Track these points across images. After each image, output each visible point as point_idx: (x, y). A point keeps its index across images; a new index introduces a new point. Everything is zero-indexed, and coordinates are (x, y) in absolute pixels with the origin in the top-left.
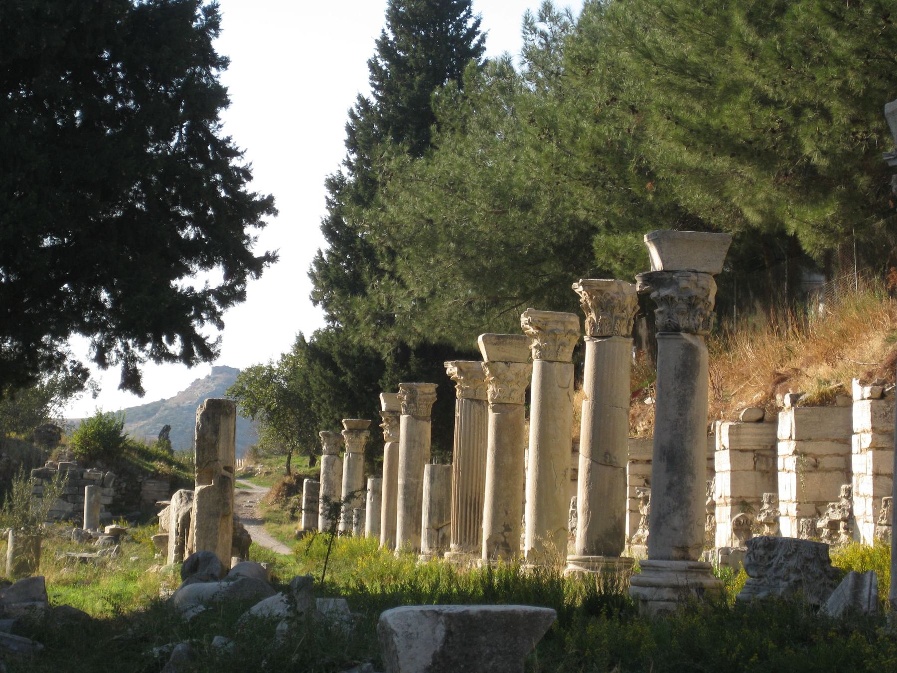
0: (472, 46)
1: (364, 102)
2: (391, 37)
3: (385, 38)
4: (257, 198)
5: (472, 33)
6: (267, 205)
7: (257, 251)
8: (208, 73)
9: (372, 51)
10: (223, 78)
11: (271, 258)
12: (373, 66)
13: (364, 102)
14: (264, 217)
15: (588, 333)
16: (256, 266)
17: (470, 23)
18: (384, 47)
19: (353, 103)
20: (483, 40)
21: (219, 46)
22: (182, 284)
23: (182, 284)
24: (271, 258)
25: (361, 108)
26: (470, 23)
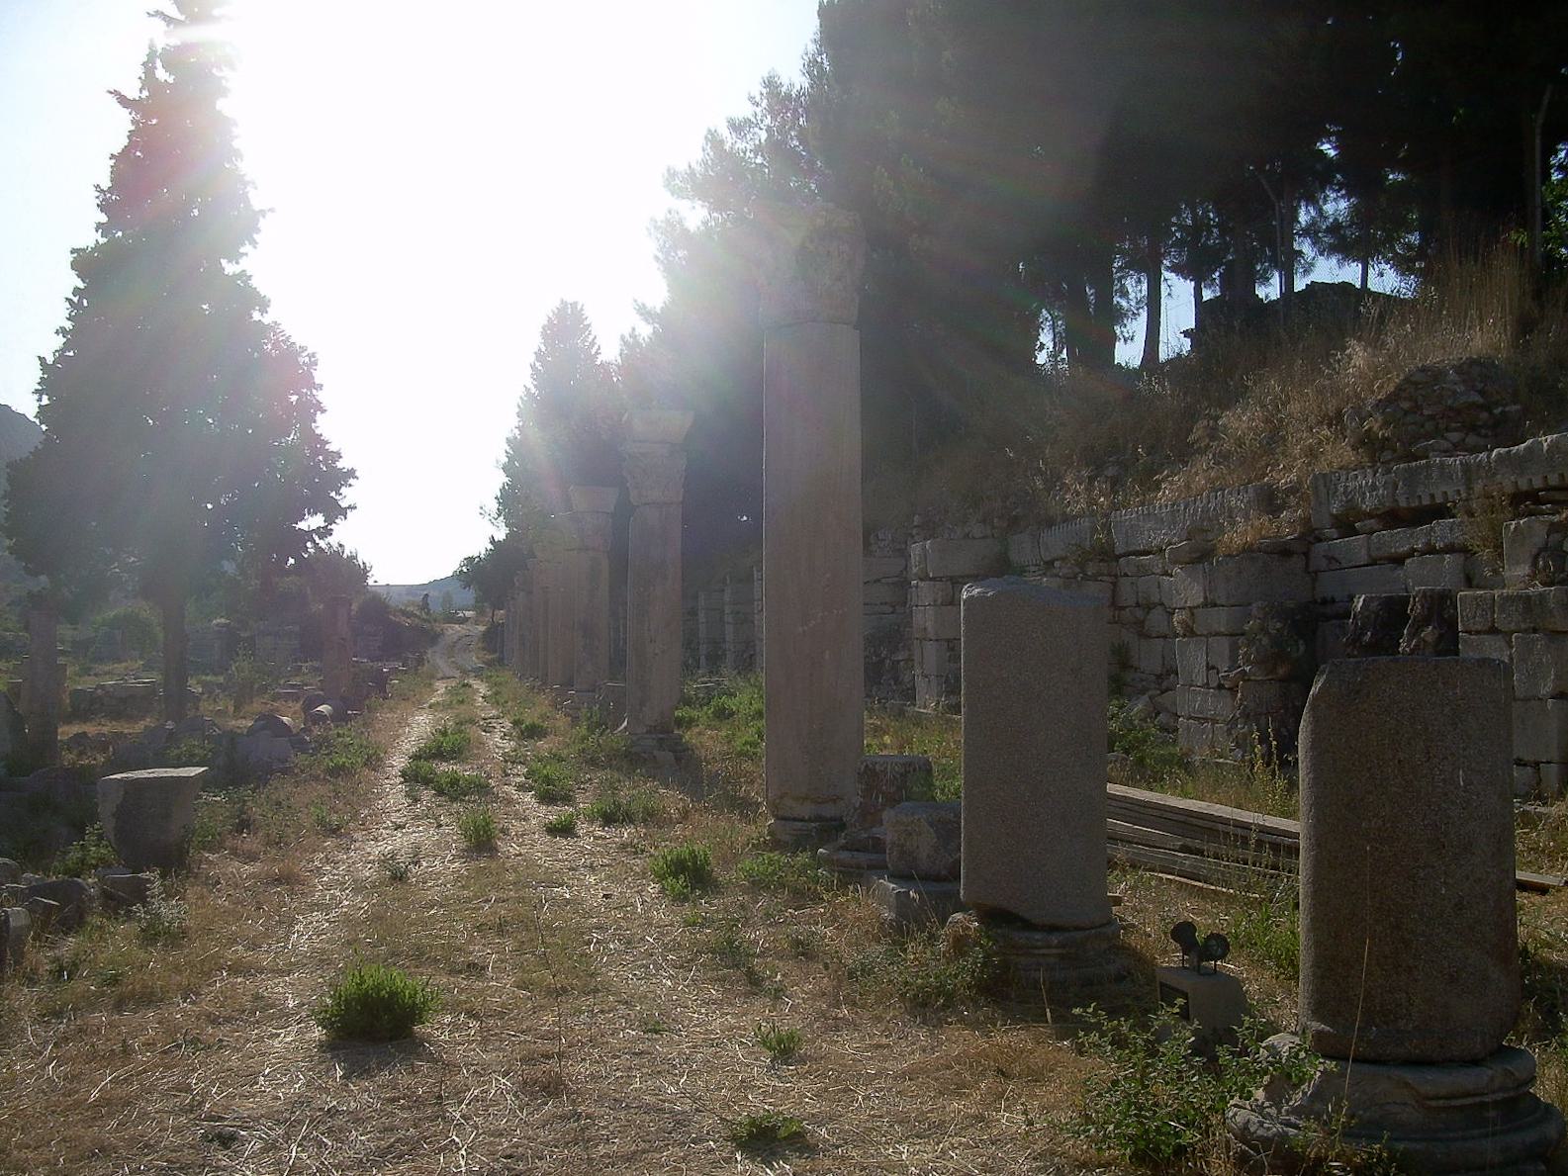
0: (593, 353)
1: (528, 390)
2: (543, 349)
3: (540, 350)
4: (345, 470)
5: (593, 343)
6: (351, 473)
7: (344, 504)
8: (311, 393)
9: (533, 358)
10: (321, 396)
11: (352, 508)
12: (533, 367)
13: (528, 390)
14: (351, 481)
15: (1556, 518)
16: (343, 512)
17: (591, 337)
18: (539, 355)
19: (521, 392)
20: (599, 348)
21: (319, 376)
22: (302, 525)
23: (302, 525)
24: (352, 508)
25: (525, 398)
26: (591, 337)
